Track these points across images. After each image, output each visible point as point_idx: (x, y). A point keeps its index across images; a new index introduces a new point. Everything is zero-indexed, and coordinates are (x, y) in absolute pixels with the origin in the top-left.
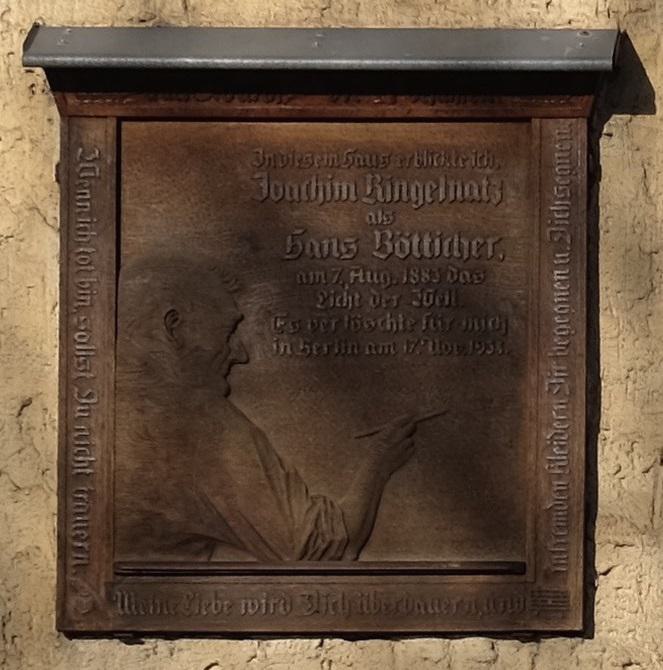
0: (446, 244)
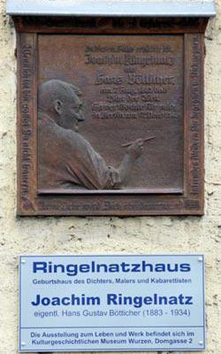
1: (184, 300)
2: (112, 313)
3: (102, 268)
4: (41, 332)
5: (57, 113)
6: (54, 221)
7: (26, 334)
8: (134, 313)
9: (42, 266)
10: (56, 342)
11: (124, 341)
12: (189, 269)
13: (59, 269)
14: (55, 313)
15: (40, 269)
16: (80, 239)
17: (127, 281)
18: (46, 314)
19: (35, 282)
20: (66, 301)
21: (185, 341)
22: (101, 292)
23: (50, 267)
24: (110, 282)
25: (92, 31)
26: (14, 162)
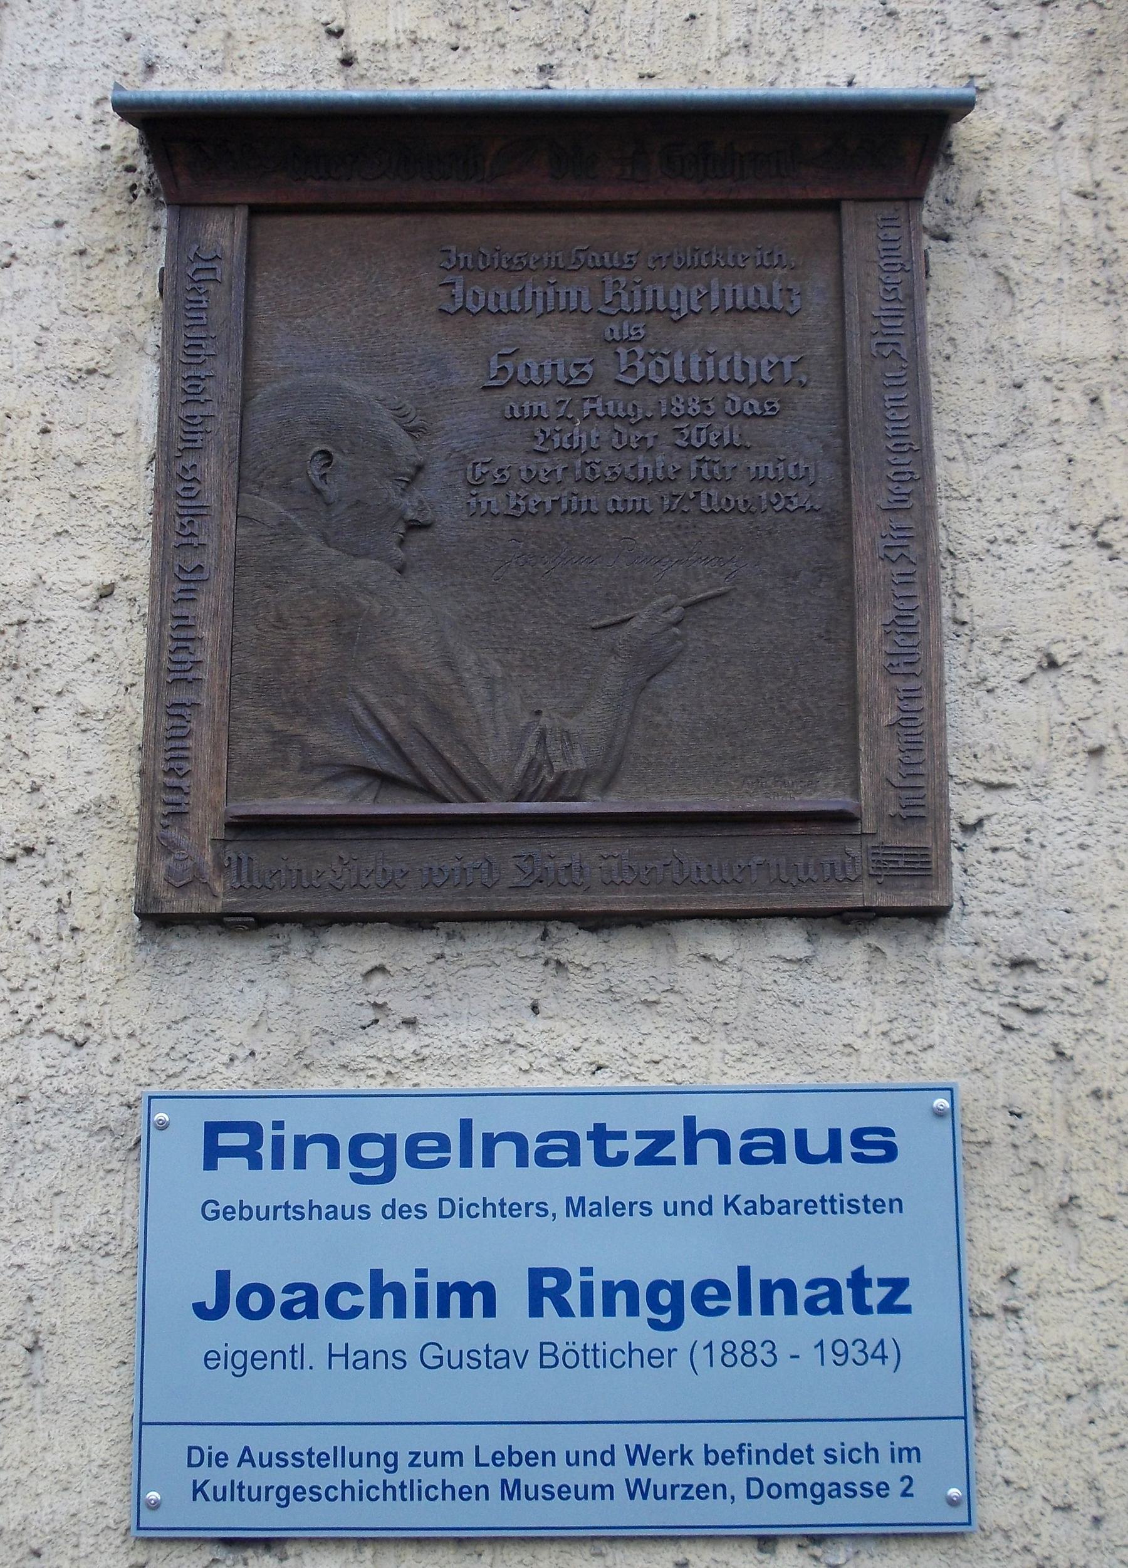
0: (723, 364)
1: (874, 1295)
2: (550, 1356)
3: (505, 1151)
4: (231, 1442)
5: (318, 492)
6: (299, 943)
7: (170, 1447)
8: (654, 1358)
9: (242, 1139)
10: (298, 1493)
11: (606, 1490)
12: (891, 1153)
13: (317, 1153)
14: (295, 1357)
15: (233, 1152)
16: (410, 1023)
17: (617, 1209)
18: (256, 1360)
19: (215, 1212)
20: (345, 1301)
21: (882, 1489)
22: (500, 1255)
23: (278, 1142)
24: (542, 1209)
25: (470, 192)
26: (135, 705)
